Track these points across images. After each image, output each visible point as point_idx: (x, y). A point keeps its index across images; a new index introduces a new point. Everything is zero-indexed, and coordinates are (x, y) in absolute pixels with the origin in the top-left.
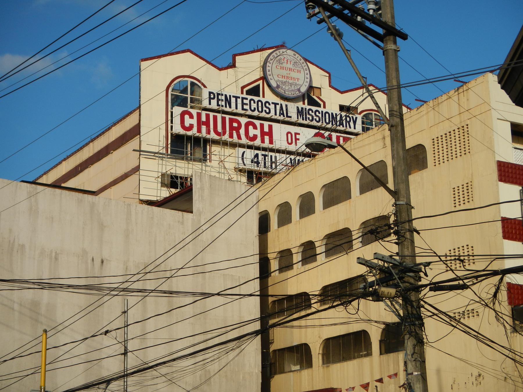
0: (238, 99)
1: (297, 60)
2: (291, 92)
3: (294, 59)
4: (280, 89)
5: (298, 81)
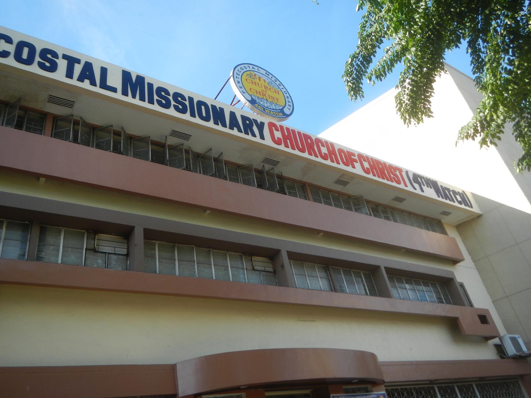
2: (272, 111)
3: (268, 78)
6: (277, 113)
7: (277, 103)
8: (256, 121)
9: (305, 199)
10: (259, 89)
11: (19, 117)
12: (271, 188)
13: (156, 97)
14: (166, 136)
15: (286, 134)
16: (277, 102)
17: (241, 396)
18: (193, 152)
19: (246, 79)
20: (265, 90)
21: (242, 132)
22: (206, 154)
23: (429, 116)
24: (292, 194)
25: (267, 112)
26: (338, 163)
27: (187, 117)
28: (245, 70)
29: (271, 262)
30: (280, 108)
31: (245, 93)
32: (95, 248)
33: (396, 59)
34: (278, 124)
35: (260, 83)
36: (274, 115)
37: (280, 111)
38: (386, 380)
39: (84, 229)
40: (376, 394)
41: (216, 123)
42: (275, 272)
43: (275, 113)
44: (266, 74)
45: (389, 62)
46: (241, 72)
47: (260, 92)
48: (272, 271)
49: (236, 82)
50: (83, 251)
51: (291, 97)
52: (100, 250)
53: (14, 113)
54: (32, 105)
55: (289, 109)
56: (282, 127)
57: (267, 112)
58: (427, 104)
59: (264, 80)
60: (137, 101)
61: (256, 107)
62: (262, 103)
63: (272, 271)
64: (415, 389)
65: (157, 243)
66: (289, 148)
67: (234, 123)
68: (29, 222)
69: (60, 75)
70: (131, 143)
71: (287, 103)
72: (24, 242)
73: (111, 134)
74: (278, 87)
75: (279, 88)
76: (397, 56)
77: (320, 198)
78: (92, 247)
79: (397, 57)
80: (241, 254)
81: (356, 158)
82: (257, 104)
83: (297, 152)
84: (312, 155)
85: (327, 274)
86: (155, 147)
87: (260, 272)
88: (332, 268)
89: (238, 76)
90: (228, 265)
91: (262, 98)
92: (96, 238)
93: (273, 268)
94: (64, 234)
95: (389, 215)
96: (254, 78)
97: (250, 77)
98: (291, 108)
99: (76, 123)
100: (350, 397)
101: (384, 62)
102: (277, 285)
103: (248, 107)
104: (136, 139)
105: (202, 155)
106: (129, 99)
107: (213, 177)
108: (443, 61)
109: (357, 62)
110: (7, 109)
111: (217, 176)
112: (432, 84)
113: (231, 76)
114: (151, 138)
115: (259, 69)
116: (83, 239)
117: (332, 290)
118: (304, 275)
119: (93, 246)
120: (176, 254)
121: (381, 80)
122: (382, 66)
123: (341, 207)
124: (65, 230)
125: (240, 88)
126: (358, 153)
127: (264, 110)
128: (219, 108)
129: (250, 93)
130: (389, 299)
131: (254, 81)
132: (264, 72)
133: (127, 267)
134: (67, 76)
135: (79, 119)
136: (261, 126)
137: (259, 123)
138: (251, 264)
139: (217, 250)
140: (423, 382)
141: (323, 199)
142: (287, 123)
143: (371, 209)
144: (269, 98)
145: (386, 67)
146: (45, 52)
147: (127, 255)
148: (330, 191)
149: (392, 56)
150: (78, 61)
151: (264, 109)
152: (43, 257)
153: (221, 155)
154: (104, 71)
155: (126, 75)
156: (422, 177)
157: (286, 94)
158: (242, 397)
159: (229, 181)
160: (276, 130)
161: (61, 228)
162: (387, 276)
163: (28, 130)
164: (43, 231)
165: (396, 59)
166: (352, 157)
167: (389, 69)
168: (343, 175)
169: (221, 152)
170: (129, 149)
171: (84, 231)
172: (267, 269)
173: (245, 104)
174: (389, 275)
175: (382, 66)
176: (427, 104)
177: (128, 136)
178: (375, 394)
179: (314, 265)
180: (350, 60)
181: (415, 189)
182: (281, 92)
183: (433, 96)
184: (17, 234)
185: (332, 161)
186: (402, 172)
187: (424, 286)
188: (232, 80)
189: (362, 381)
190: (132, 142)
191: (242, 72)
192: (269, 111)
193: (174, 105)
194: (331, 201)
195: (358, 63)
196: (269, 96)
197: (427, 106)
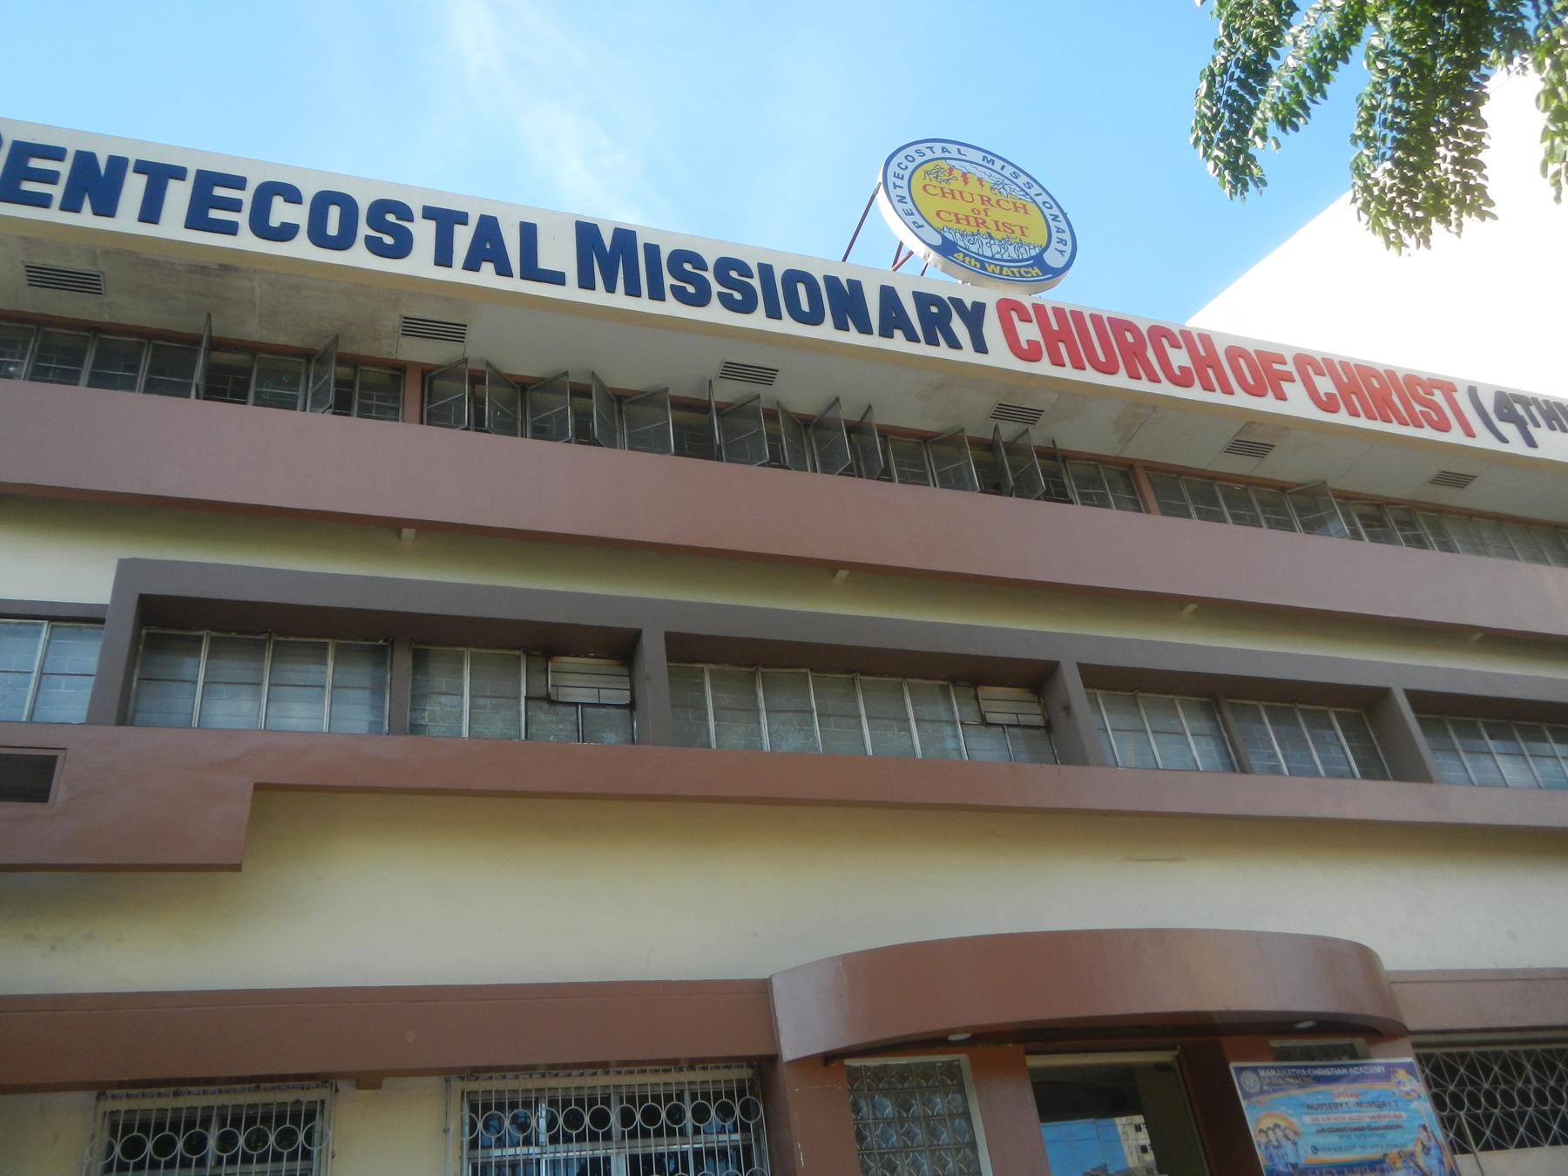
0: (458, 229)
1: (1003, 178)
2: (1009, 267)
3: (992, 173)
4: (962, 255)
5: (1023, 234)
6: (1022, 270)
7: (1023, 241)
8: (958, 303)
9: (1136, 511)
10: (963, 208)
11: (338, 383)
12: (1024, 489)
13: (669, 280)
14: (710, 381)
15: (1055, 327)
16: (1023, 238)
17: (957, 1063)
18: (786, 413)
19: (924, 187)
20: (982, 208)
21: (919, 341)
22: (828, 415)
23: (1482, 215)
24: (1093, 500)
25: (993, 272)
26: (1228, 391)
27: (757, 320)
28: (919, 160)
29: (1036, 699)
30: (1033, 253)
31: (922, 226)
32: (548, 694)
33: (1329, 56)
34: (1027, 301)
35: (966, 190)
36: (1015, 276)
37: (1032, 262)
38: (1412, 1025)
39: (518, 649)
40: (1381, 1065)
41: (841, 325)
42: (1048, 727)
43: (1015, 270)
44: (984, 160)
45: (1308, 70)
46: (907, 167)
47: (967, 218)
48: (1042, 723)
49: (895, 199)
50: (519, 702)
51: (1065, 215)
52: (561, 699)
53: (327, 377)
54: (364, 349)
55: (1061, 252)
56: (1039, 309)
57: (993, 272)
58: (1475, 174)
59: (980, 180)
60: (619, 300)
61: (957, 263)
62: (974, 248)
63: (1042, 723)
64: (1529, 1054)
65: (707, 668)
66: (1064, 365)
67: (893, 318)
68: (385, 640)
69: (420, 263)
70: (620, 413)
71: (1055, 235)
72: (377, 691)
73: (566, 395)
74: (1022, 193)
75: (1027, 194)
76: (1332, 47)
77: (1184, 501)
78: (541, 692)
79: (1335, 49)
80: (945, 683)
81: (1290, 367)
82: (960, 252)
83: (1090, 376)
84: (1140, 378)
85: (1217, 722)
86: (685, 416)
87: (1004, 729)
88: (1232, 704)
89: (899, 182)
90: (907, 714)
91: (975, 232)
92: (549, 669)
93: (1043, 715)
94: (471, 664)
95: (1423, 530)
96: (948, 180)
97: (937, 177)
98: (1068, 249)
99: (477, 379)
100: (1293, 1070)
101: (1294, 74)
102: (1057, 763)
103: (936, 266)
104: (633, 399)
105: (815, 420)
106: (598, 296)
107: (853, 476)
108: (1523, 24)
109: (1228, 84)
110: (312, 368)
111: (864, 474)
112: (1480, 108)
113: (880, 184)
114: (671, 392)
115: (963, 149)
116: (519, 669)
117: (1234, 770)
118: (1141, 731)
119: (545, 688)
120: (761, 694)
121: (1296, 128)
122: (1290, 87)
123: (1255, 522)
124: (472, 653)
125: (908, 214)
126: (1294, 354)
127: (983, 267)
128: (849, 281)
129: (938, 224)
130: (1424, 786)
131: (947, 187)
132: (977, 157)
133: (633, 739)
134: (437, 263)
135: (483, 368)
136: (974, 316)
137: (969, 306)
138: (977, 708)
139: (875, 675)
140: (1548, 1035)
141: (1195, 502)
142: (1058, 296)
143: (1359, 519)
144: (998, 229)
145: (1302, 87)
146: (380, 209)
147: (631, 706)
148: (1215, 477)
149: (1315, 51)
150: (462, 218)
151: (982, 263)
152: (426, 725)
153: (868, 415)
154: (529, 233)
155: (587, 234)
156: (1525, 401)
157: (1051, 208)
158: (959, 1066)
159: (900, 482)
160: (1021, 320)
161: (461, 649)
162: (1418, 718)
163: (365, 412)
164: (420, 661)
165: (1329, 56)
166: (1276, 366)
167: (1312, 92)
168: (1250, 424)
169: (867, 406)
170: (618, 429)
171: (517, 653)
172: (1023, 719)
173: (925, 257)
174: (1420, 716)
175: (1290, 87)
176: (1475, 174)
177: (609, 393)
178: (1377, 1065)
179: (1173, 700)
180: (1204, 86)
181: (1504, 440)
182: (1034, 204)
183: (1488, 147)
184: (361, 673)
185: (1205, 389)
186: (1456, 391)
187: (1557, 741)
188: (881, 195)
189: (1328, 1025)
190: (624, 408)
191: (912, 166)
192: (998, 267)
193: (720, 295)
194: (1220, 507)
195: (1230, 87)
196: (996, 222)
197: (1475, 179)
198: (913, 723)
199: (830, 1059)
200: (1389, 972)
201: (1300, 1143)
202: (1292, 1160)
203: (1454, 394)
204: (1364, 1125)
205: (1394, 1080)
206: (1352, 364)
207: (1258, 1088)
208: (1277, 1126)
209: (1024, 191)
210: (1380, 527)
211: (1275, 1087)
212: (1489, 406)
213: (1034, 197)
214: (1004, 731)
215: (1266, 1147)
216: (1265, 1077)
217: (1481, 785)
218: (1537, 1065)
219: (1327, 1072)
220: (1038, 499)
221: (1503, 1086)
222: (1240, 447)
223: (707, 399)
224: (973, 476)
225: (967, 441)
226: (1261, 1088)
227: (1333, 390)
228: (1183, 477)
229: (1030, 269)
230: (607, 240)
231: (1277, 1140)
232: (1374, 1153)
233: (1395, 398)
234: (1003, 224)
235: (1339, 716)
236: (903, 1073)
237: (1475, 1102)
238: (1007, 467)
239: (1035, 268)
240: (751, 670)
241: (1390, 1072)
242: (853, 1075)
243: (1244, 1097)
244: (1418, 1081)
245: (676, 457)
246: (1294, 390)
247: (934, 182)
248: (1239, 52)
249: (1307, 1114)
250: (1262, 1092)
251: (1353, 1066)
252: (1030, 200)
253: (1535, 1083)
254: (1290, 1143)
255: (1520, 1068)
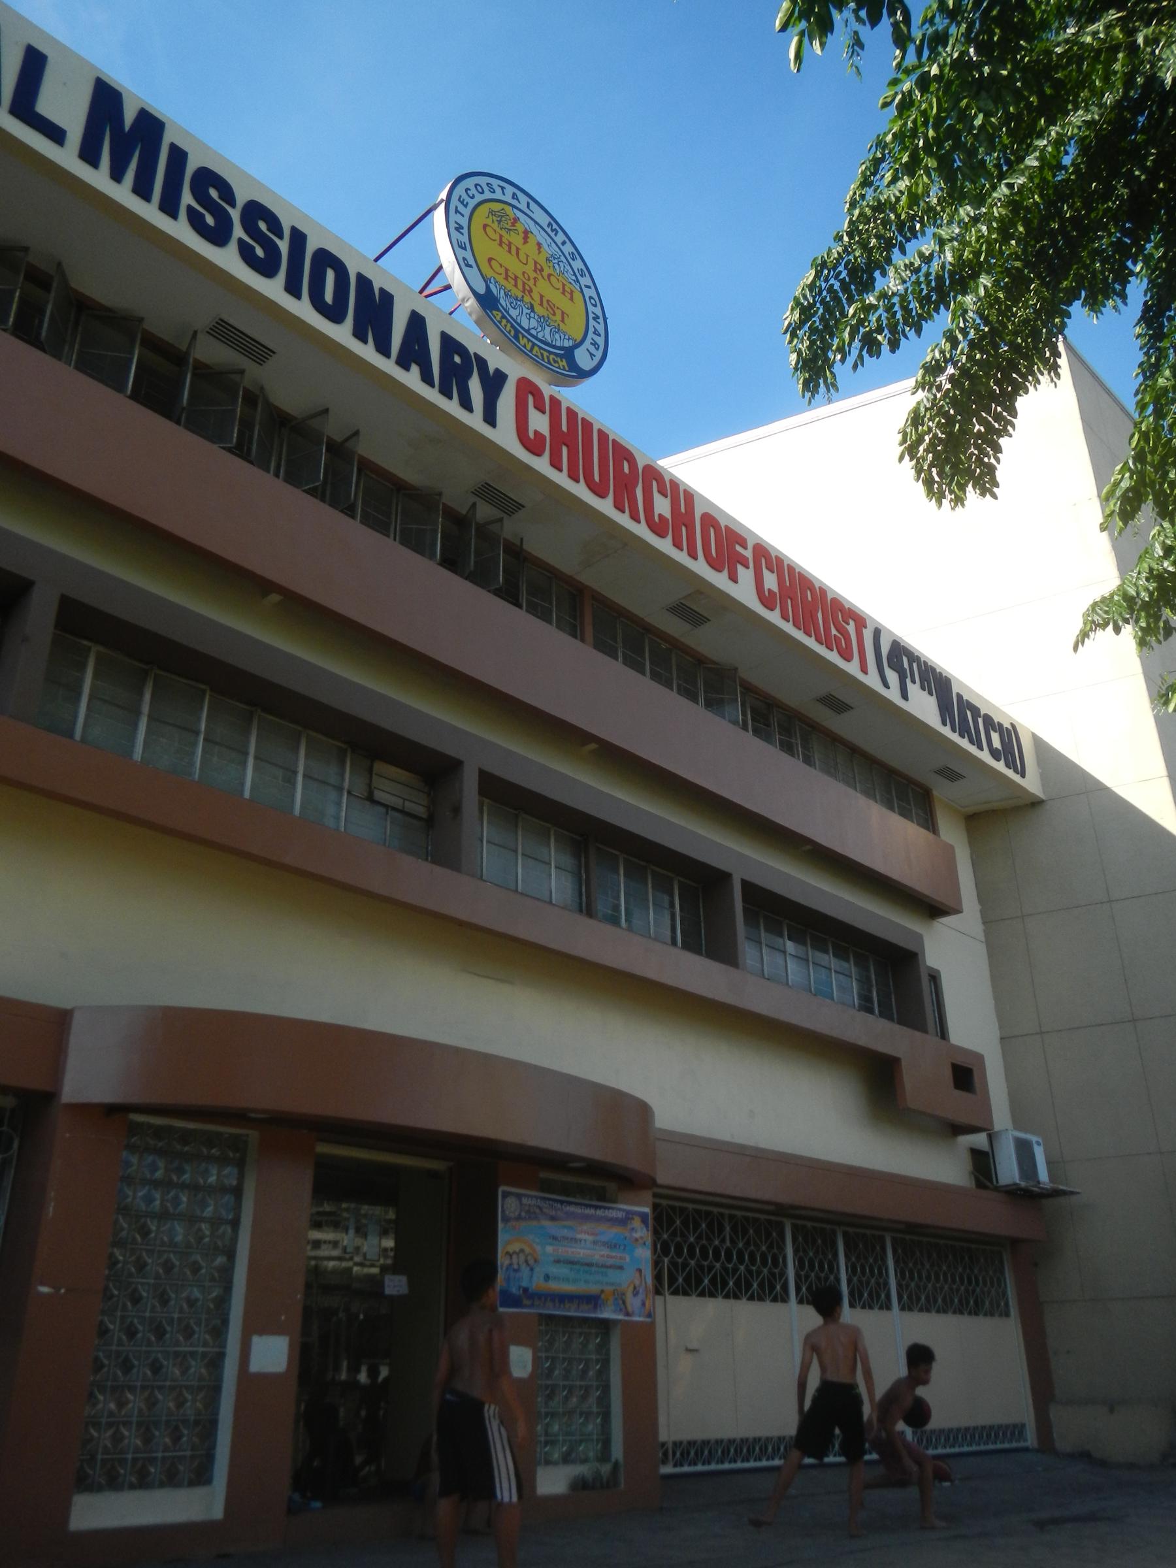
2: (540, 348)
4: (500, 315)
6: (552, 357)
8: (482, 363)
10: (516, 268)
12: (480, 577)
16: (562, 325)
18: (268, 404)
19: (485, 226)
26: (693, 555)
27: (273, 288)
28: (488, 195)
30: (567, 344)
31: (470, 266)
34: (547, 390)
35: (524, 249)
36: (543, 360)
38: (661, 1180)
40: (624, 1210)
43: (545, 354)
47: (516, 278)
49: (453, 225)
56: (555, 403)
57: (525, 346)
59: (539, 245)
60: (122, 194)
62: (514, 313)
64: (731, 1217)
65: (95, 649)
74: (574, 278)
75: (578, 281)
77: (616, 643)
81: (748, 554)
83: (580, 490)
85: (580, 861)
89: (461, 208)
91: (520, 297)
96: (510, 230)
98: (599, 354)
103: (470, 314)
106: (99, 178)
109: (832, 281)
113: (442, 201)
114: (146, 326)
117: (581, 911)
118: (513, 851)
120: (147, 697)
123: (668, 684)
125: (460, 247)
127: (516, 337)
131: (506, 237)
132: (544, 220)
142: (574, 396)
144: (541, 304)
148: (647, 629)
156: (913, 658)
166: (738, 548)
172: (410, 807)
173: (464, 300)
178: (620, 1210)
182: (581, 294)
186: (866, 627)
189: (594, 1169)
191: (479, 198)
196: (542, 297)
198: (300, 778)
199: (113, 1111)
200: (660, 1130)
201: (537, 1269)
202: (524, 1284)
203: (864, 630)
204: (594, 1261)
205: (629, 1227)
206: (797, 571)
207: (517, 1214)
208: (522, 1251)
209: (576, 276)
210: (765, 725)
211: (531, 1215)
212: (885, 649)
213: (583, 287)
214: (387, 813)
215: (507, 1269)
216: (526, 1205)
217: (768, 979)
218: (734, 1229)
219: (578, 1210)
220: (489, 591)
221: (704, 1242)
222: (681, 610)
223: (184, 348)
224: (436, 544)
225: (325, 440)
226: (520, 1215)
227: (775, 589)
228: (622, 619)
229: (559, 360)
230: (129, 117)
231: (518, 1264)
232: (593, 1289)
233: (820, 615)
234: (548, 301)
235: (680, 882)
236: (186, 1137)
237: (679, 1252)
238: (473, 549)
239: (564, 360)
240: (145, 667)
241: (629, 1219)
242: (134, 1129)
243: (503, 1220)
244: (648, 1230)
245: (131, 402)
246: (746, 575)
247: (495, 225)
248: (852, 255)
249: (551, 1244)
250: (519, 1218)
251: (600, 1207)
252: (578, 288)
253: (728, 1243)
254: (528, 1269)
255: (721, 1230)
